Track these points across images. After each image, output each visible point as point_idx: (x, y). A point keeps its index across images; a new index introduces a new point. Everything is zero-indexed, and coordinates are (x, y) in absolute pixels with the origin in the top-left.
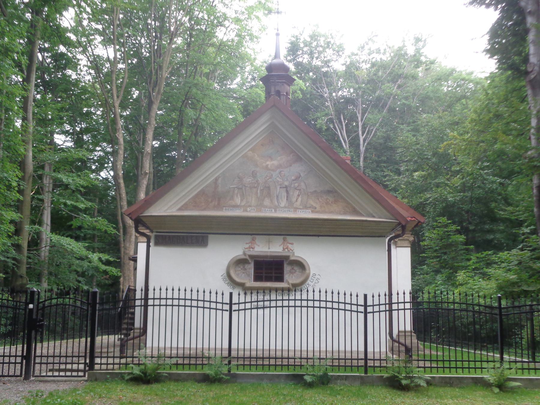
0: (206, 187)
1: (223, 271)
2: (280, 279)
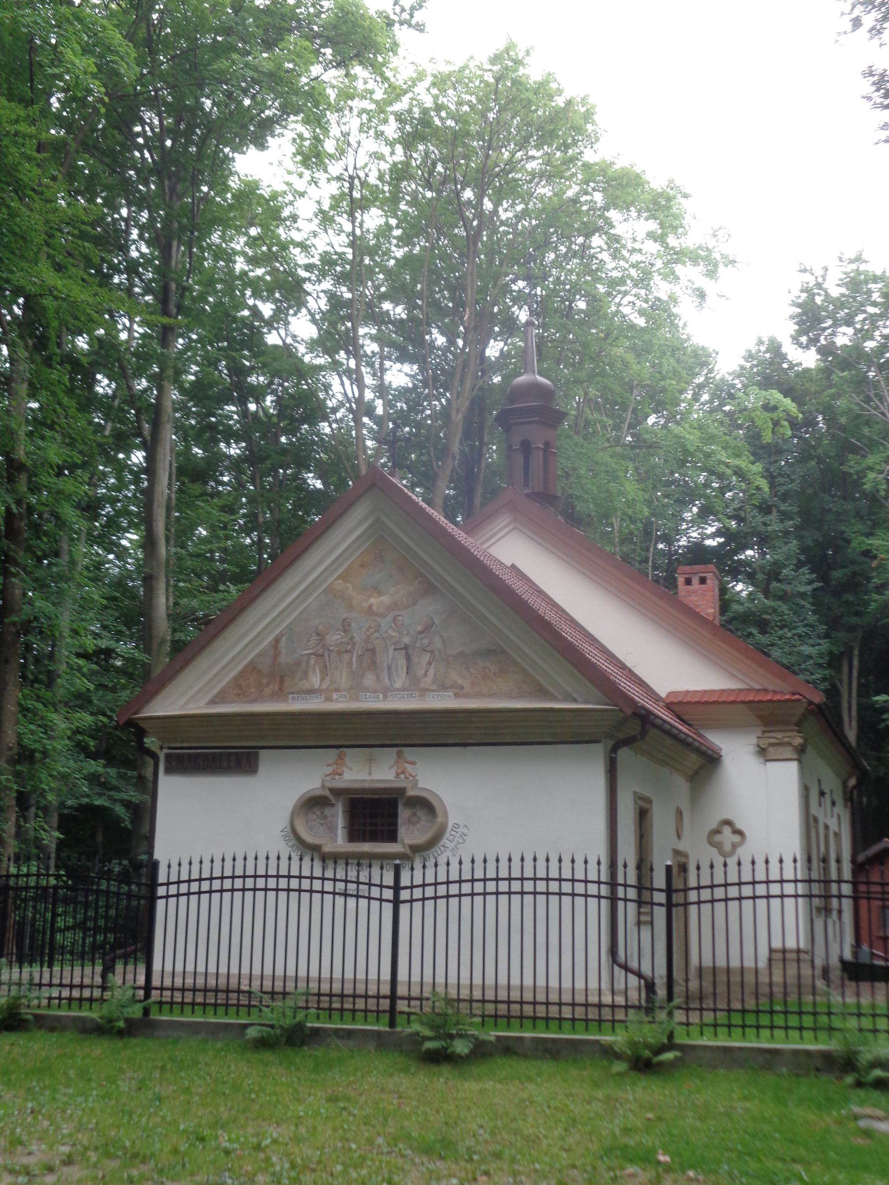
0: (260, 655)
1: (285, 823)
2: (392, 836)
